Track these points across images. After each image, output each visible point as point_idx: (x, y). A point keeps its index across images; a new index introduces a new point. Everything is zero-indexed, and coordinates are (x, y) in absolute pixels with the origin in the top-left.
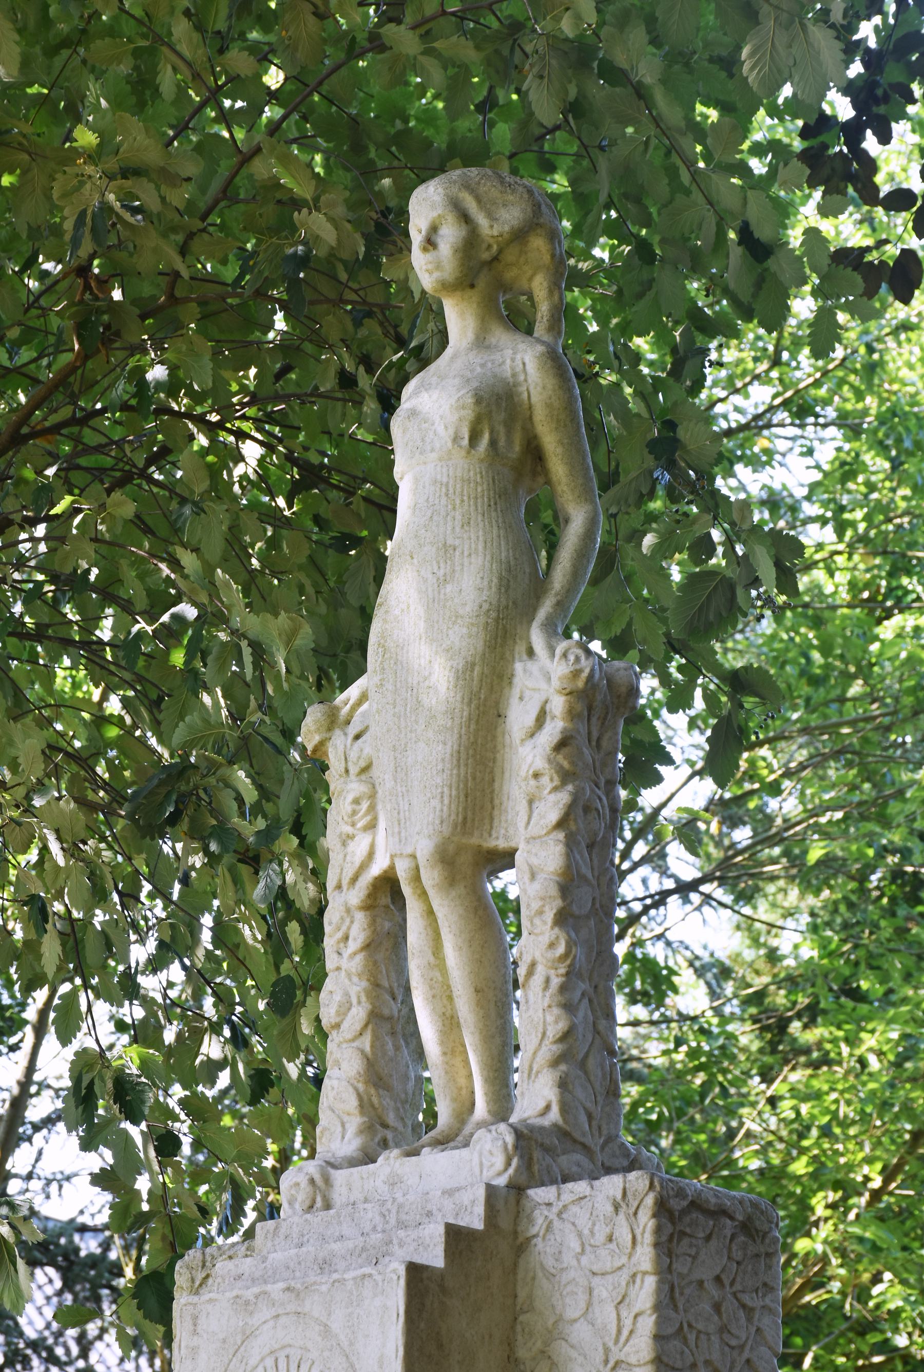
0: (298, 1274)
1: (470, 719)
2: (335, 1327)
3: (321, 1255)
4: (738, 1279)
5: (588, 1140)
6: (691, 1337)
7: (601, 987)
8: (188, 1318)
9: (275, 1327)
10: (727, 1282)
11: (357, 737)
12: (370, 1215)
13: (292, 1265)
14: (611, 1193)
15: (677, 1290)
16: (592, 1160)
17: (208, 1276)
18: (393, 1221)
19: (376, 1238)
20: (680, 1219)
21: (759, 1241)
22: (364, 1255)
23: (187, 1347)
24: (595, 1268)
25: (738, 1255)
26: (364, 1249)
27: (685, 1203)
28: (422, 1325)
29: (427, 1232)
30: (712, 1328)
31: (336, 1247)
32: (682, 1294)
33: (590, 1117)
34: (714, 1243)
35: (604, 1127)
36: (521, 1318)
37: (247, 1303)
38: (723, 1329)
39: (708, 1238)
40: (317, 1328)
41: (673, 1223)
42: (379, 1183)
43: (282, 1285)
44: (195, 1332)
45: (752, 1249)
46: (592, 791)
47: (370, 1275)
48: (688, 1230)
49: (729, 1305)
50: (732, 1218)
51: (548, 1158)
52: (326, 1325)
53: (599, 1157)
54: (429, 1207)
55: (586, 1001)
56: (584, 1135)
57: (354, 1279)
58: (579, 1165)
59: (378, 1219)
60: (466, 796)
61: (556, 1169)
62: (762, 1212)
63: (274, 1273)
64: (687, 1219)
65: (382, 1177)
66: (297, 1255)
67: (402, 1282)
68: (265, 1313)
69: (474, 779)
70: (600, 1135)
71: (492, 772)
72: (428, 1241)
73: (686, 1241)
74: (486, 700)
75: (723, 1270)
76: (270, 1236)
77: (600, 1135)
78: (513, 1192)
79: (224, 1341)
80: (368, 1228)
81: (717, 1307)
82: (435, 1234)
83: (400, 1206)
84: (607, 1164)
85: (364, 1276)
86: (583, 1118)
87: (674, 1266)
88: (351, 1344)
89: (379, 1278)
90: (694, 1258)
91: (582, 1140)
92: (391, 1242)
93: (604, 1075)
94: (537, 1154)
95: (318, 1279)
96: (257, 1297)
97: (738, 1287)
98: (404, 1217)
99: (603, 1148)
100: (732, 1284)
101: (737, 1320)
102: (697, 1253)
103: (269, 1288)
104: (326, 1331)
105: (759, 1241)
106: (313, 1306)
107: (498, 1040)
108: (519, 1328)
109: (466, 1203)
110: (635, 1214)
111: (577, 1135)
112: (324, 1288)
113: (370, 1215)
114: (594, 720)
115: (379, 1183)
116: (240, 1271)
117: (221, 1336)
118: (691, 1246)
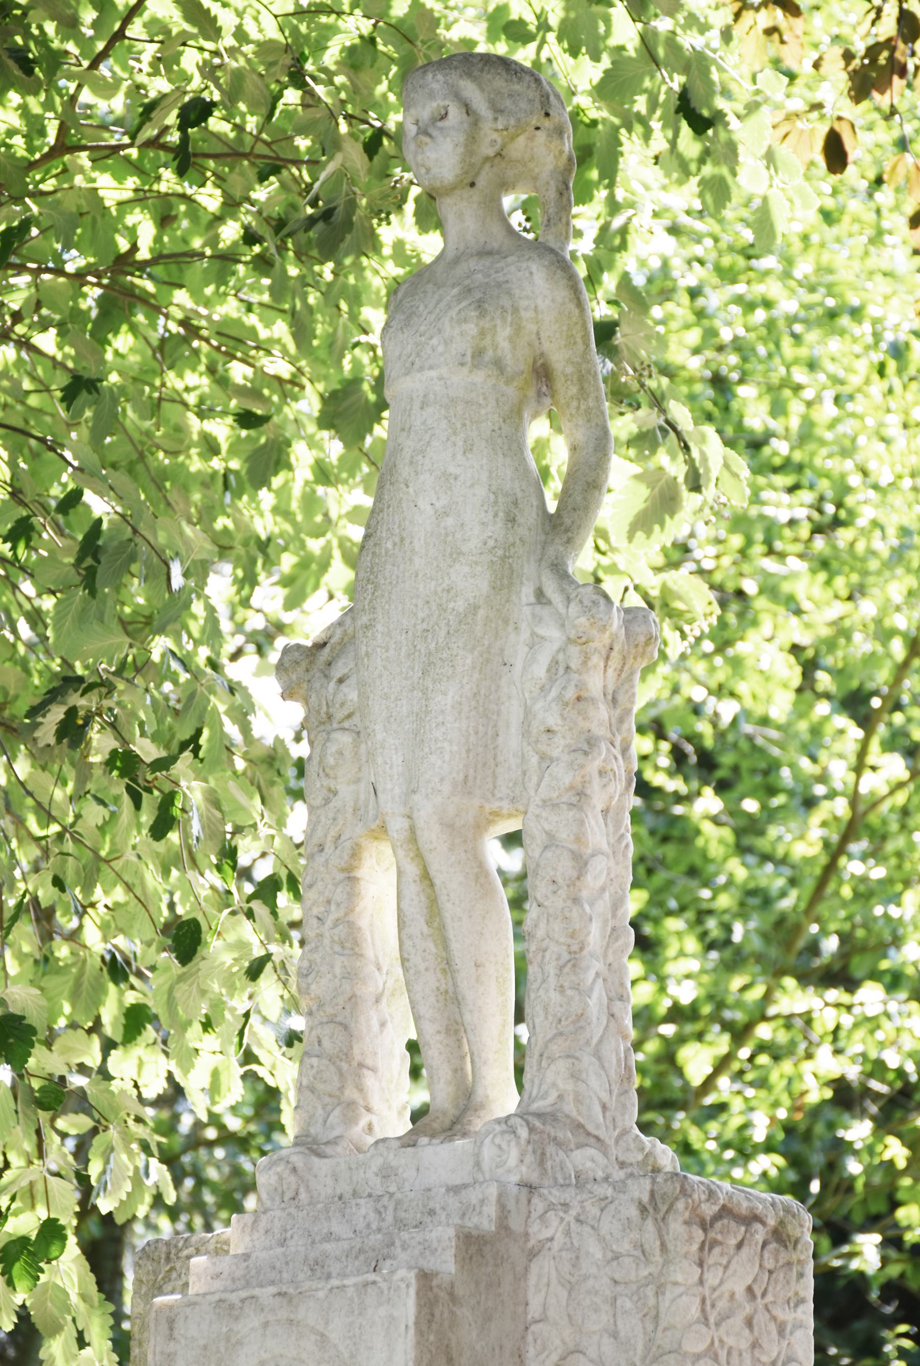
0: (285, 1275)
1: (474, 668)
2: (334, 1337)
3: (312, 1255)
4: (770, 1289)
5: (602, 1133)
6: (723, 1355)
7: (615, 965)
8: (164, 1321)
9: (264, 1335)
10: (758, 1293)
11: (341, 681)
12: (363, 1211)
13: (278, 1265)
14: (636, 1194)
15: (708, 1302)
16: (605, 1154)
17: (172, 1269)
18: (389, 1218)
19: (376, 1239)
20: (712, 1225)
21: (790, 1247)
22: (362, 1257)
23: (162, 1353)
24: (617, 1277)
25: (769, 1264)
26: (361, 1251)
27: (716, 1208)
28: (432, 1338)
29: (434, 1234)
30: (744, 1345)
31: (328, 1247)
32: (713, 1306)
33: (604, 1107)
34: (745, 1250)
35: (619, 1118)
36: (533, 1328)
37: (232, 1307)
38: (755, 1345)
39: (740, 1246)
40: (313, 1337)
41: (705, 1230)
42: (370, 1174)
43: (272, 1290)
44: (171, 1337)
45: (784, 1256)
46: (608, 750)
47: (374, 1283)
48: (719, 1237)
49: (761, 1318)
50: (764, 1224)
51: (561, 1153)
52: (322, 1335)
53: (614, 1151)
54: (431, 1205)
55: (600, 981)
56: (598, 1127)
57: (355, 1285)
58: (593, 1161)
59: (372, 1216)
60: (468, 751)
61: (569, 1165)
62: (794, 1216)
63: (258, 1273)
64: (718, 1225)
65: (374, 1169)
66: (284, 1254)
67: (412, 1291)
68: (251, 1321)
69: (477, 733)
70: (615, 1128)
71: (495, 726)
72: (435, 1244)
73: (717, 1250)
74: (490, 646)
75: (755, 1280)
76: (248, 1230)
77: (615, 1128)
78: (525, 1191)
79: (205, 1348)
80: (361, 1225)
81: (749, 1323)
82: (443, 1235)
83: (398, 1203)
84: (621, 1159)
85: (366, 1285)
86: (597, 1109)
87: (705, 1276)
88: (352, 1356)
89: (384, 1286)
90: (726, 1267)
91: (596, 1132)
92: (393, 1244)
93: (619, 1061)
94: (551, 1149)
95: (314, 1284)
96: (243, 1301)
97: (769, 1298)
98: (402, 1215)
99: (617, 1142)
100: (764, 1295)
101: (769, 1333)
102: (729, 1262)
103: (257, 1292)
104: (323, 1338)
105: (790, 1247)
106: (308, 1313)
107: (430, 981)
108: (530, 1338)
109: (474, 1201)
110: (664, 1219)
111: (590, 1128)
112: (321, 1294)
113: (363, 1211)
114: (610, 671)
115: (370, 1174)
116: (218, 1270)
117: (202, 1342)
118: (722, 1254)
